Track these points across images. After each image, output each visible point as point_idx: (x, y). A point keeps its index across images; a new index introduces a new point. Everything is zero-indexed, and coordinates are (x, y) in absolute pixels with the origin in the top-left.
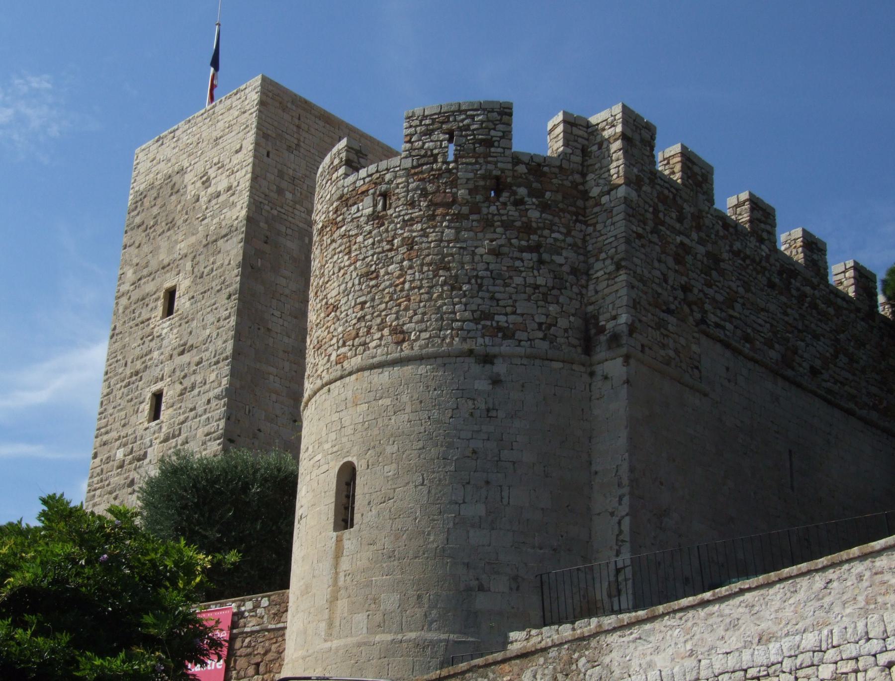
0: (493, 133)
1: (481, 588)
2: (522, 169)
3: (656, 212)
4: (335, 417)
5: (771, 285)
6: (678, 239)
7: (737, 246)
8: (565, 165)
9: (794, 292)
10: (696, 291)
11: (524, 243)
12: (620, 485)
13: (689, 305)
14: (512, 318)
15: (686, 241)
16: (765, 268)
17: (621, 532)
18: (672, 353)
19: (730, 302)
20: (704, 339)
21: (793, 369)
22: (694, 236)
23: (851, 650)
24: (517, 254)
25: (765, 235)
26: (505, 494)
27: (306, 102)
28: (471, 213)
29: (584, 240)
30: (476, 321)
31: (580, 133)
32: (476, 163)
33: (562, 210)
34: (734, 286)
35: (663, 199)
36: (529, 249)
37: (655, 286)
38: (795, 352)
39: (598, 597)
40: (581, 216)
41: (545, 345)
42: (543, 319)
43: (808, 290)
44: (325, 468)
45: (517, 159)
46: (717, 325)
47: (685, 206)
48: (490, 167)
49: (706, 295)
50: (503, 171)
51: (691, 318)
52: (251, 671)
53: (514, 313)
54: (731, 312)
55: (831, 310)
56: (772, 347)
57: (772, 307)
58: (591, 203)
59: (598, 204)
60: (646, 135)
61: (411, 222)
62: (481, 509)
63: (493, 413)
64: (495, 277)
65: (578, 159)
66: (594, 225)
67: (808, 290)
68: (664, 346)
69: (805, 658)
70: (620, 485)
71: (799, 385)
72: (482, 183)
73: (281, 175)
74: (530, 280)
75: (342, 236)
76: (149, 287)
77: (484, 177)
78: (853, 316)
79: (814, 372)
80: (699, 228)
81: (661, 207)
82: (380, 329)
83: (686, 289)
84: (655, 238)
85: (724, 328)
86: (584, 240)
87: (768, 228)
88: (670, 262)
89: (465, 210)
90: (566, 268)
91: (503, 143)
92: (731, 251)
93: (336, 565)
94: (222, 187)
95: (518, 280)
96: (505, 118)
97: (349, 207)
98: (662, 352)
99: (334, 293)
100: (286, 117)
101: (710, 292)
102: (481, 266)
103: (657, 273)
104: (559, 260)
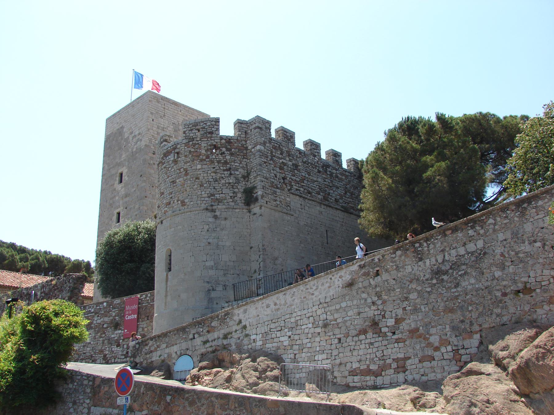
0: (213, 129)
1: (213, 290)
2: (223, 141)
3: (272, 152)
4: (164, 233)
5: (319, 172)
6: (281, 161)
7: (305, 159)
8: (239, 138)
9: (328, 173)
10: (288, 179)
11: (225, 168)
12: (259, 251)
13: (285, 184)
14: (221, 195)
15: (284, 161)
16: (316, 166)
17: (260, 267)
18: (278, 203)
19: (302, 180)
20: (291, 195)
21: (328, 201)
22: (288, 159)
23: (299, 313)
24: (222, 172)
25: (316, 154)
26: (220, 257)
27: (167, 98)
28: (207, 158)
29: (246, 165)
30: (209, 197)
31: (244, 126)
32: (208, 140)
33: (238, 155)
34: (304, 174)
35: (275, 148)
36: (227, 170)
37: (271, 180)
38: (329, 194)
39: (254, 289)
40: (245, 156)
41: (233, 204)
42: (232, 195)
43: (334, 171)
44: (162, 250)
45: (222, 138)
46: (297, 190)
47: (284, 148)
48: (212, 141)
49: (292, 179)
50: (217, 143)
51: (286, 189)
52: (146, 319)
53: (222, 193)
54: (302, 184)
55: (344, 177)
56: (319, 194)
57: (319, 180)
58: (248, 151)
59: (251, 152)
60: (267, 125)
61: (186, 163)
62: (212, 263)
63: (216, 229)
64: (216, 180)
65: (244, 136)
66: (250, 159)
67: (334, 171)
68: (276, 201)
69: (287, 316)
70: (259, 251)
71: (330, 207)
72: (210, 148)
73: (158, 128)
74: (227, 181)
75: (165, 167)
76: (113, 172)
77: (210, 145)
78: (352, 178)
79: (336, 201)
80: (289, 156)
81: (274, 151)
82: (178, 201)
83: (284, 178)
84: (271, 162)
85: (300, 190)
86: (246, 165)
87: (318, 151)
88: (278, 170)
89: (204, 158)
90: (240, 176)
91: (217, 132)
92: (303, 162)
93: (167, 284)
94: (137, 133)
95: (223, 181)
96: (217, 123)
97: (166, 157)
98: (275, 203)
99: (163, 188)
100: (160, 105)
101: (294, 178)
102: (211, 177)
103: (273, 175)
104: (237, 173)
